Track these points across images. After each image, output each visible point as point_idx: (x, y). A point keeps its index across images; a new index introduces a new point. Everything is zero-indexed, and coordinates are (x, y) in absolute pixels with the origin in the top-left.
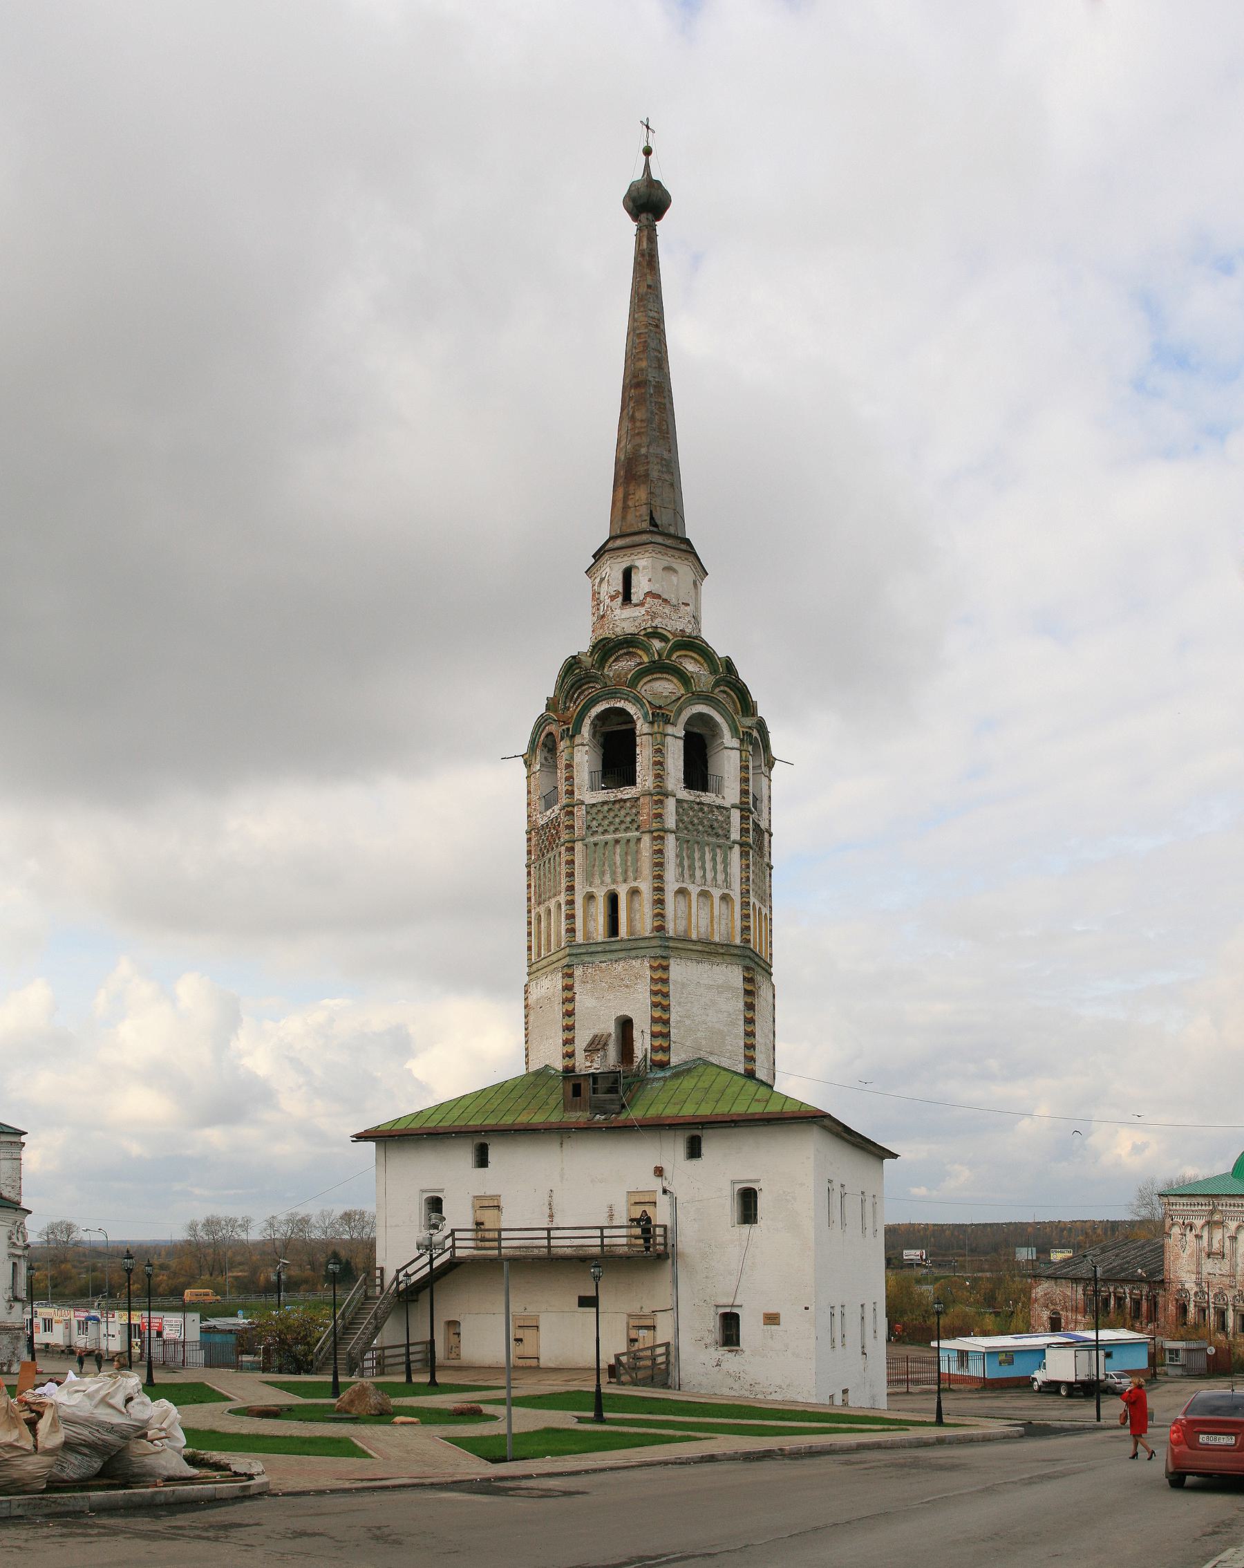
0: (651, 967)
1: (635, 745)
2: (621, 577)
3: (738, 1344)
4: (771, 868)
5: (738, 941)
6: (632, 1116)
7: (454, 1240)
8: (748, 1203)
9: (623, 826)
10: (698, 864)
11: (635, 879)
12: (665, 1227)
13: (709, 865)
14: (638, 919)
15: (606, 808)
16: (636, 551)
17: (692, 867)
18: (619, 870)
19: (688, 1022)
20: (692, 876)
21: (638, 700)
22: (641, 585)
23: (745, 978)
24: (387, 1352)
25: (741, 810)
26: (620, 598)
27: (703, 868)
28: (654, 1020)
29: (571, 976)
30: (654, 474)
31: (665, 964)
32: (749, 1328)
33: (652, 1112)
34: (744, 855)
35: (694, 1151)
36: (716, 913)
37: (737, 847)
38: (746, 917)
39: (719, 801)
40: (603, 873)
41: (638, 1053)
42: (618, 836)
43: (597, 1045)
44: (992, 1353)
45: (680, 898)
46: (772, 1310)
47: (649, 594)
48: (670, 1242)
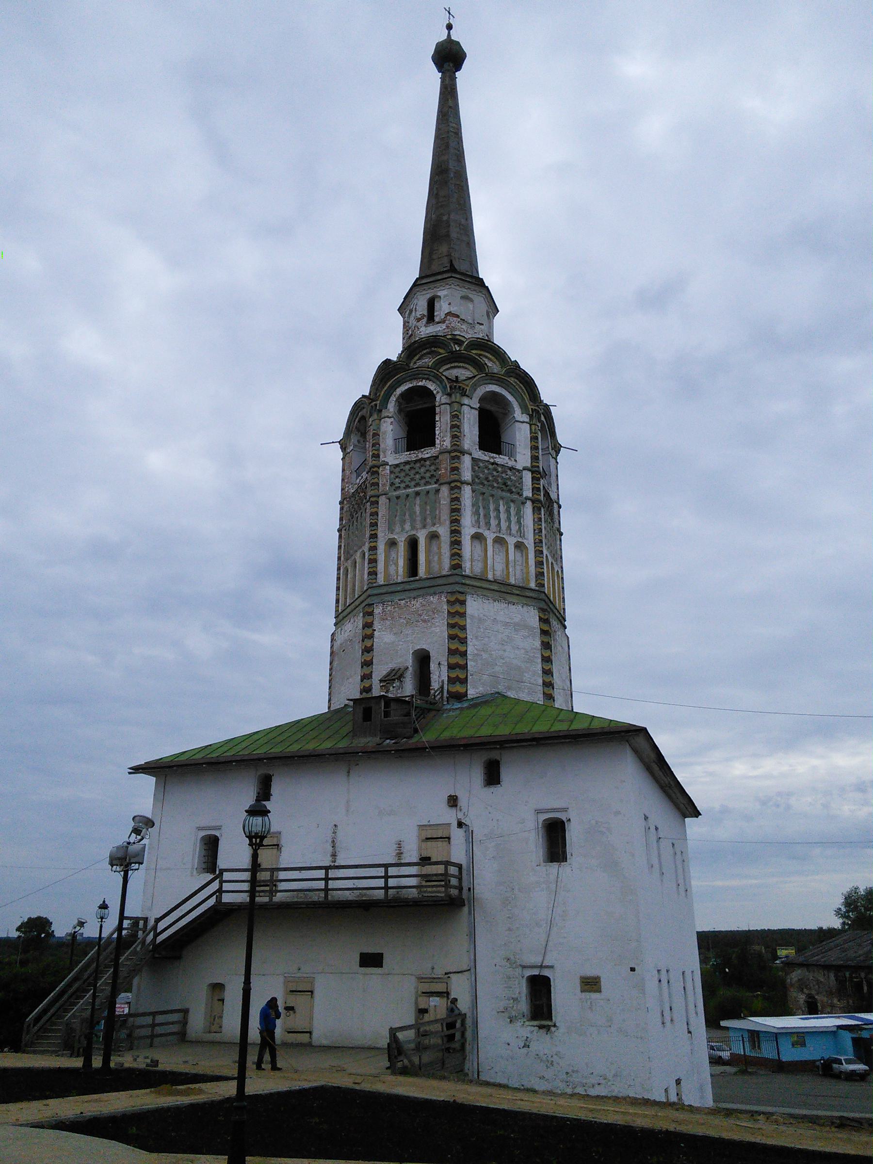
1: (435, 414)
2: (426, 304)
3: (550, 1018)
4: (561, 534)
5: (533, 585)
6: (424, 739)
7: (221, 883)
8: (555, 838)
11: (434, 525)
12: (460, 867)
13: (503, 516)
14: (434, 560)
15: (408, 467)
16: (438, 284)
17: (487, 516)
18: (418, 519)
19: (485, 656)
20: (488, 524)
21: (437, 378)
22: (442, 308)
23: (540, 619)
26: (425, 319)
27: (498, 517)
28: (451, 652)
29: (371, 614)
30: (454, 235)
31: (461, 598)
32: (564, 996)
33: (446, 735)
34: (536, 510)
35: (492, 777)
36: (511, 557)
37: (529, 503)
38: (539, 564)
39: (511, 463)
40: (403, 522)
41: (435, 685)
42: (418, 489)
43: (394, 676)
45: (477, 543)
47: (449, 314)
48: (465, 885)
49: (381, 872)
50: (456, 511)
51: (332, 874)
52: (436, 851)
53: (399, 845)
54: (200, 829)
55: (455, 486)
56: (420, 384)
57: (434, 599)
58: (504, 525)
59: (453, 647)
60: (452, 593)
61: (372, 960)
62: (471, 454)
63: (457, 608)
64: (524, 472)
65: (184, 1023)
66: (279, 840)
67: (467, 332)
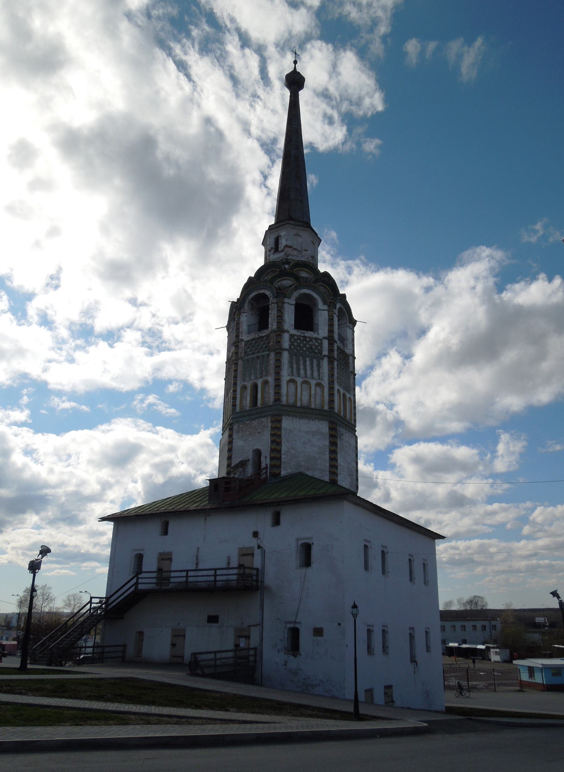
0: (271, 421)
5: (326, 408)
10: (302, 367)
11: (266, 375)
12: (257, 569)
13: (308, 368)
15: (254, 341)
17: (298, 369)
20: (299, 375)
22: (283, 242)
24: (106, 649)
28: (272, 450)
31: (279, 419)
32: (306, 638)
34: (331, 362)
36: (313, 392)
39: (315, 336)
43: (243, 464)
44: (545, 668)
46: (319, 626)
47: (286, 246)
48: (260, 579)
49: (212, 572)
52: (246, 561)
53: (229, 558)
55: (279, 354)
56: (262, 292)
58: (309, 373)
61: (213, 619)
62: (288, 332)
63: (277, 424)
65: (124, 652)
67: (297, 256)
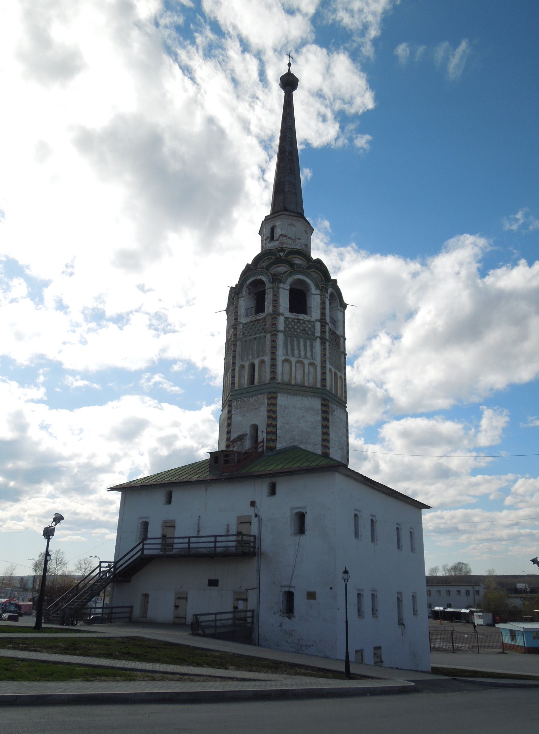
5: (319, 385)
7: (143, 545)
9: (259, 331)
11: (263, 356)
15: (251, 324)
20: (293, 355)
22: (278, 232)
25: (321, 322)
27: (299, 349)
28: (268, 425)
30: (287, 189)
31: (274, 395)
32: (299, 601)
34: (323, 343)
36: (306, 371)
43: (241, 438)
44: (526, 631)
48: (257, 546)
49: (213, 539)
50: (274, 347)
51: (218, 539)
52: (244, 529)
53: (228, 526)
54: (141, 518)
55: (274, 335)
56: (258, 278)
57: (260, 397)
58: (302, 353)
59: (269, 423)
60: (269, 393)
61: (213, 583)
62: (283, 315)
63: (272, 401)
64: (316, 323)
65: (131, 612)
66: (174, 524)
67: (291, 245)
